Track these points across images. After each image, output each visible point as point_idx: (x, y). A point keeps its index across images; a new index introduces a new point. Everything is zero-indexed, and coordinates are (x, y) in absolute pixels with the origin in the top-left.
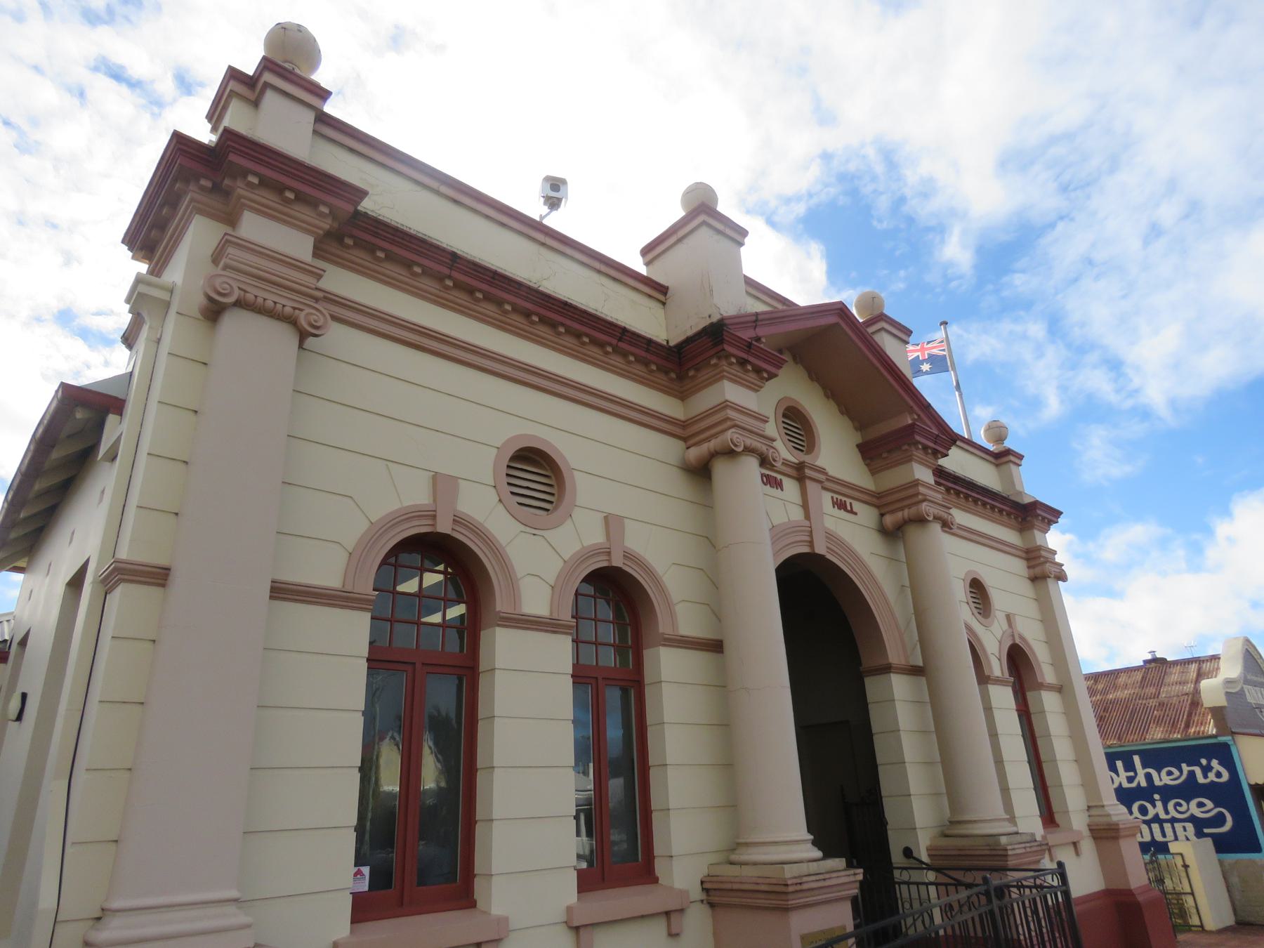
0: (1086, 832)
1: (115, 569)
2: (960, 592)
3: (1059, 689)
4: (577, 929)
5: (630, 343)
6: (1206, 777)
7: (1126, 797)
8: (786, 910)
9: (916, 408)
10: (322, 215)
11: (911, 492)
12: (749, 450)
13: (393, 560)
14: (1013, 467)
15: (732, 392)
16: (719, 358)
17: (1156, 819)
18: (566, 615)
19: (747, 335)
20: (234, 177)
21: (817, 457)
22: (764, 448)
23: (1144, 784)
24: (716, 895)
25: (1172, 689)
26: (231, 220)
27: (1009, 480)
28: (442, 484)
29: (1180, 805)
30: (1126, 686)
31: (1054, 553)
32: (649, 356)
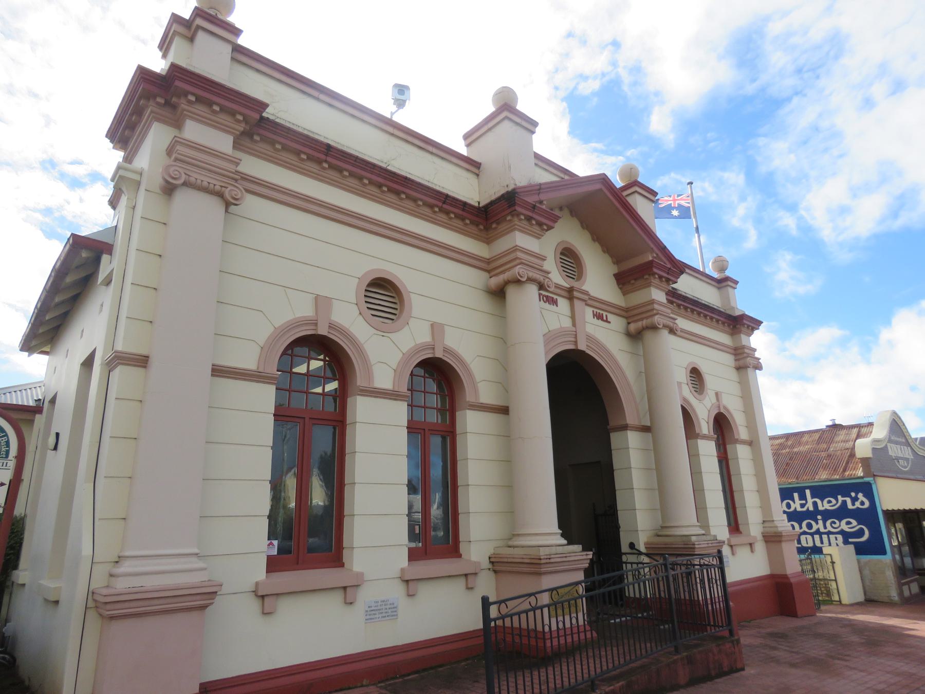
0: (760, 537)
1: (115, 357)
2: (682, 376)
3: (750, 443)
4: (407, 581)
5: (451, 205)
6: (853, 504)
7: (794, 517)
8: (540, 574)
9: (655, 248)
10: (238, 121)
11: (649, 307)
12: (530, 280)
13: (290, 352)
14: (730, 290)
15: (522, 240)
16: (513, 216)
17: (818, 532)
18: (404, 388)
19: (531, 199)
20: (179, 97)
21: (583, 284)
22: (541, 279)
23: (811, 509)
24: (498, 565)
25: (839, 445)
26: (178, 124)
27: (726, 299)
29: (835, 523)
30: (807, 443)
31: (755, 350)
32: (465, 214)
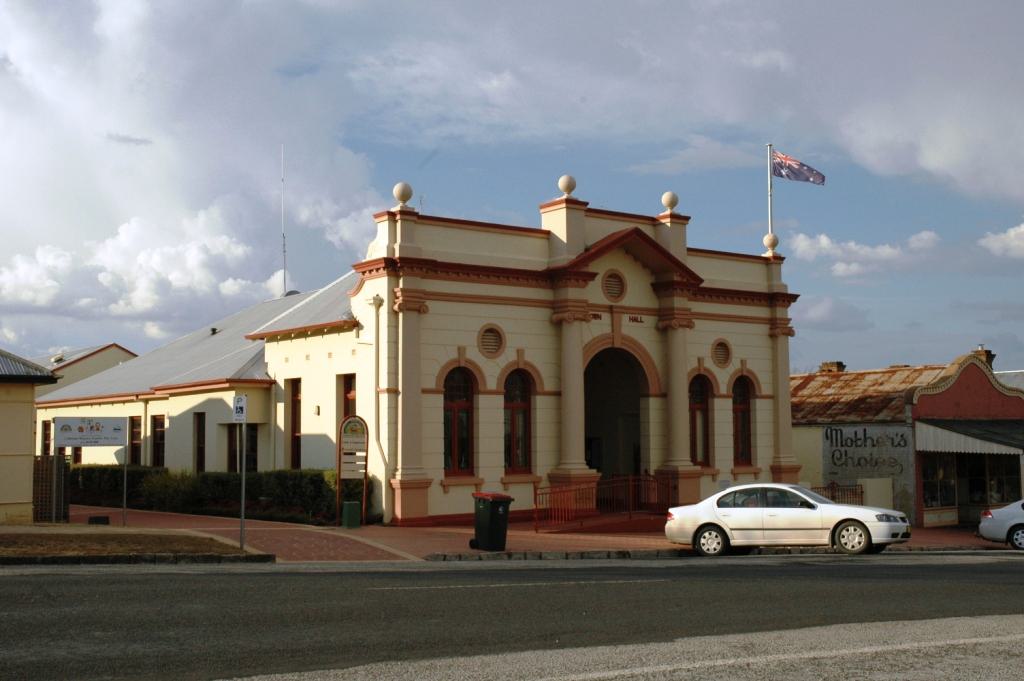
28: (461, 350)
